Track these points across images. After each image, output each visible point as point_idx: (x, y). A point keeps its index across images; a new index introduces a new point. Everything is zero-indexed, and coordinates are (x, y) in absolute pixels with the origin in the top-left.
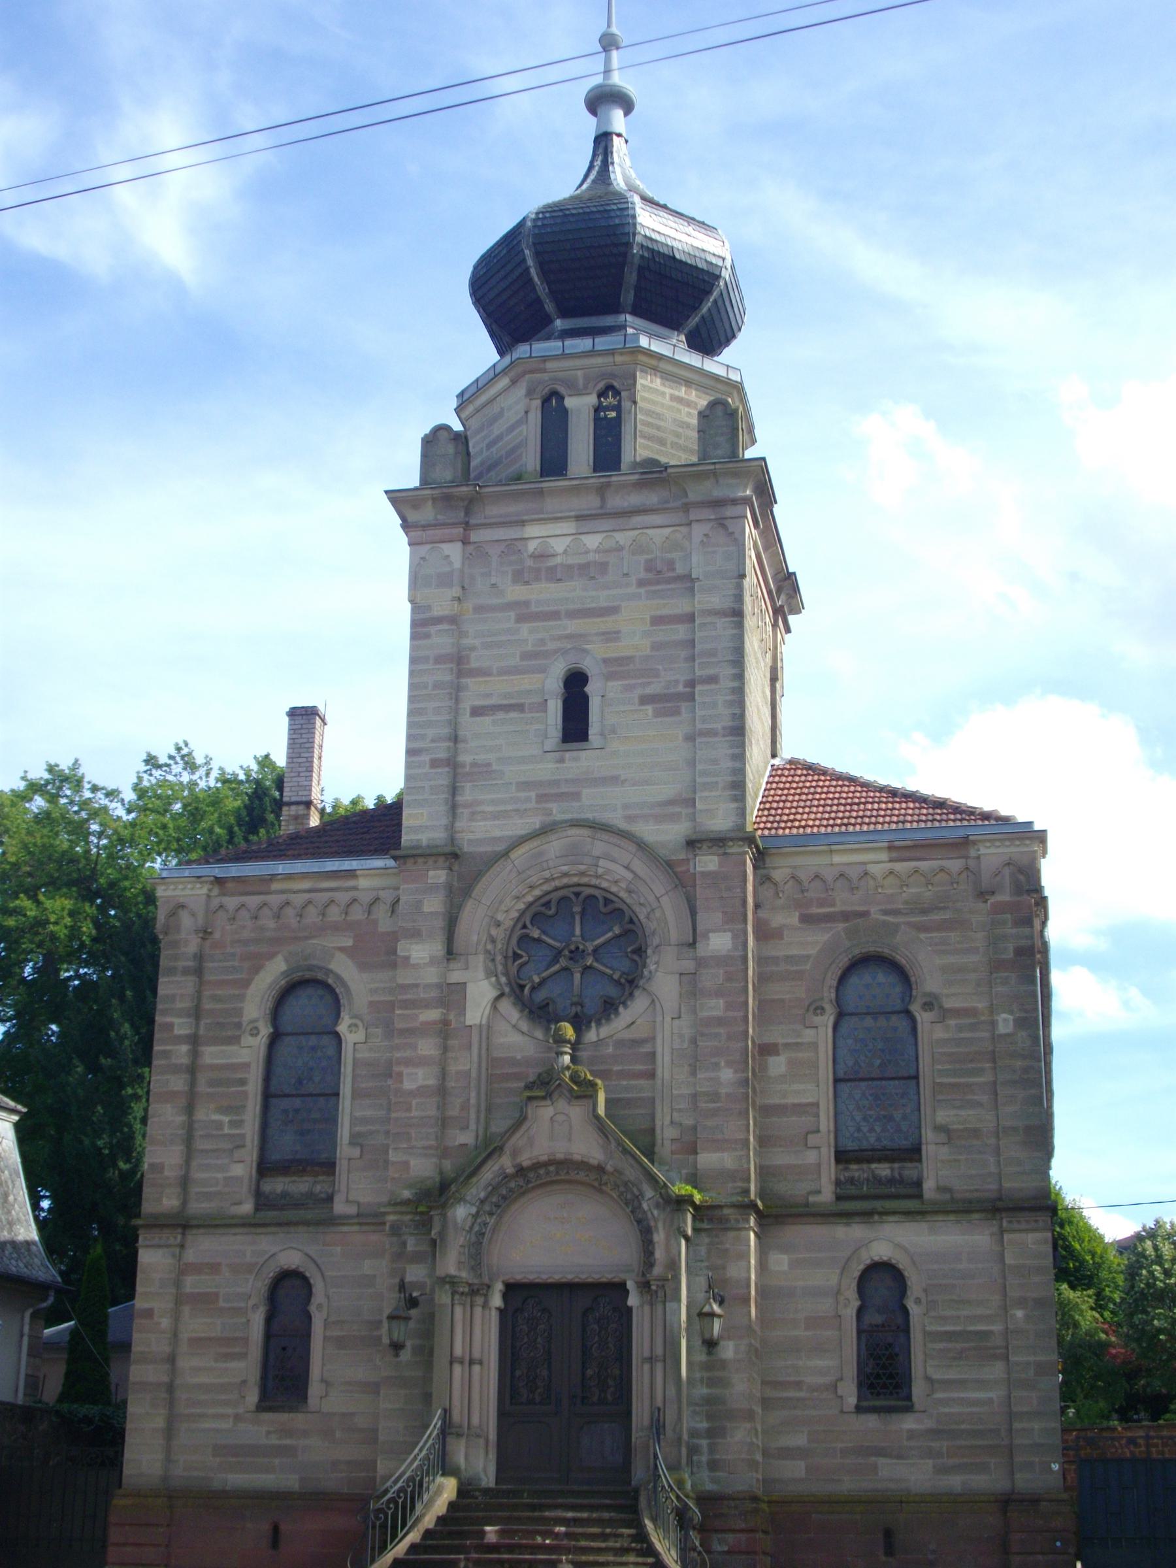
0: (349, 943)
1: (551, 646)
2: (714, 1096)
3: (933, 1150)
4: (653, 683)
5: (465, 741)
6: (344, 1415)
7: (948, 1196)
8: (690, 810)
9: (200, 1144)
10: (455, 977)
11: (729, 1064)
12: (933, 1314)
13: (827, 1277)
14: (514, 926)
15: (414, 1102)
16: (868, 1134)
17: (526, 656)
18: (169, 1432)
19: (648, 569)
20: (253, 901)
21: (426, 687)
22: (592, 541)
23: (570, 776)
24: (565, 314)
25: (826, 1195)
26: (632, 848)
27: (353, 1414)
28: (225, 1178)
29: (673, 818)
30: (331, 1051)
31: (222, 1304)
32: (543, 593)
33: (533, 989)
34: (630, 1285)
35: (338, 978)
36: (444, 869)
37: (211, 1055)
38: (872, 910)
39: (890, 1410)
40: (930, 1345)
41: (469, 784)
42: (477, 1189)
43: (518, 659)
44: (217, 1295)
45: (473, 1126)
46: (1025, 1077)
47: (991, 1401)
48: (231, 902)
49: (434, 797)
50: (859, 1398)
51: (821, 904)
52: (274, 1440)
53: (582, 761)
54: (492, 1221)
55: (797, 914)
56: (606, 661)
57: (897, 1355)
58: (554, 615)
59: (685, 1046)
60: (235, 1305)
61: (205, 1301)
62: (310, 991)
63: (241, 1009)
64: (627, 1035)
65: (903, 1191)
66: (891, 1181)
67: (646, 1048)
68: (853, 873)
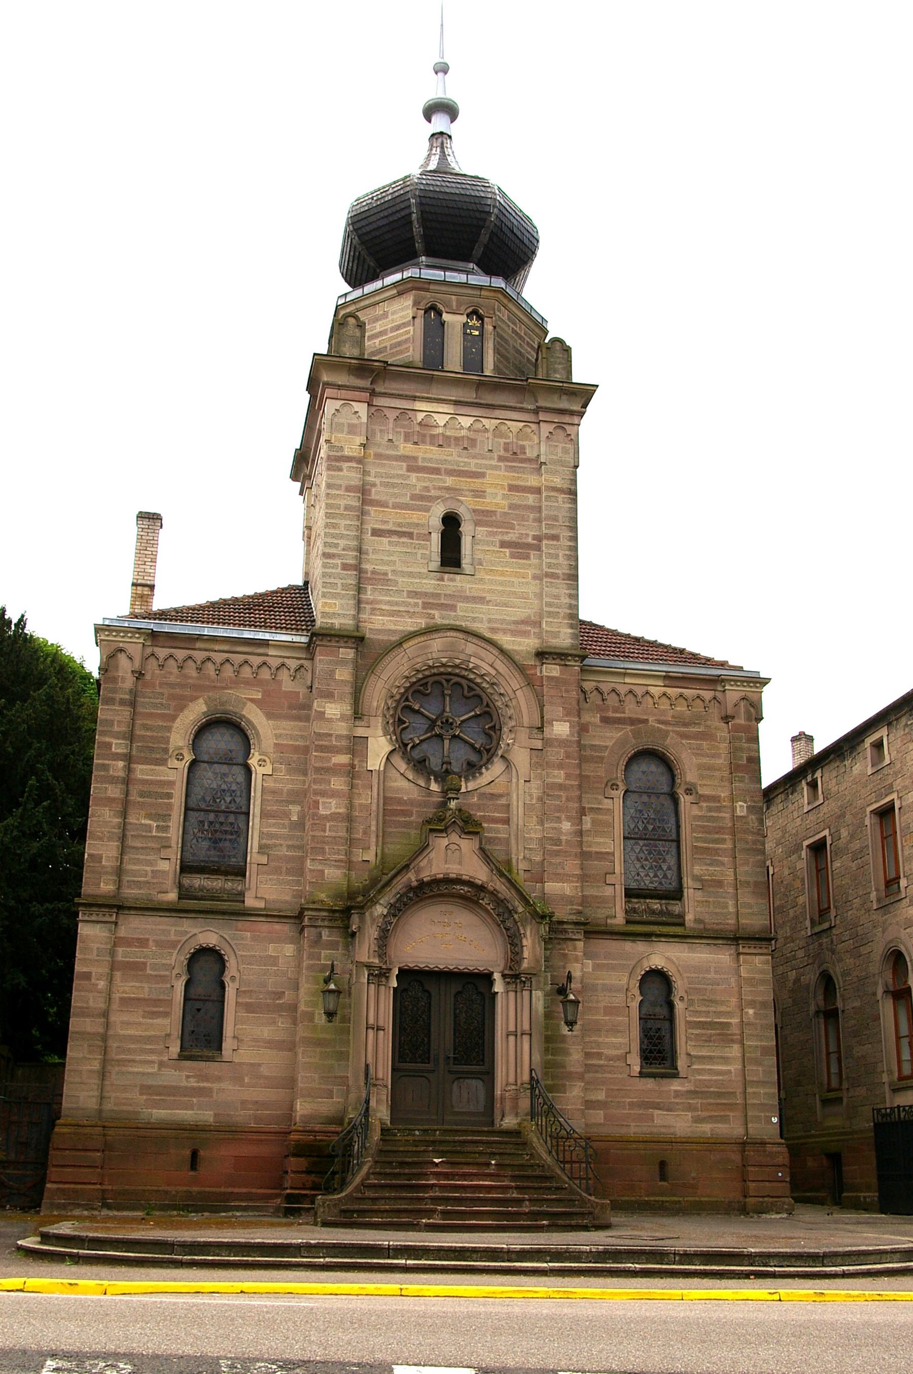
0: (259, 696)
1: (433, 493)
2: (558, 842)
3: (690, 893)
4: (509, 533)
5: (367, 554)
6: (252, 1064)
7: (701, 926)
8: (537, 630)
9: (130, 842)
10: (360, 732)
11: (568, 818)
12: (691, 1009)
13: (621, 979)
14: (400, 698)
15: (328, 825)
16: (644, 878)
17: (413, 497)
18: (103, 1074)
19: (506, 450)
20: (181, 654)
21: (339, 508)
22: (466, 422)
23: (448, 592)
24: (428, 254)
25: (619, 920)
26: (496, 652)
27: (259, 1065)
28: (152, 871)
29: (525, 634)
30: (241, 778)
31: (149, 972)
32: (428, 453)
33: (413, 747)
34: (497, 976)
35: (249, 722)
36: (352, 648)
37: (142, 771)
38: (650, 719)
39: (663, 1076)
40: (690, 1031)
41: (370, 587)
42: (389, 897)
43: (408, 499)
44: (145, 964)
45: (373, 848)
46: (754, 847)
47: (729, 1072)
48: (162, 653)
49: (344, 592)
50: (642, 1067)
51: (616, 710)
52: (193, 1083)
53: (454, 583)
54: (394, 920)
55: (599, 715)
56: (474, 511)
57: (664, 1036)
58: (436, 471)
59: (534, 802)
60: (162, 973)
61: (135, 969)
62: (223, 730)
63: (169, 738)
64: (488, 790)
65: (670, 920)
66: (661, 913)
67: (503, 801)
68: (639, 691)
